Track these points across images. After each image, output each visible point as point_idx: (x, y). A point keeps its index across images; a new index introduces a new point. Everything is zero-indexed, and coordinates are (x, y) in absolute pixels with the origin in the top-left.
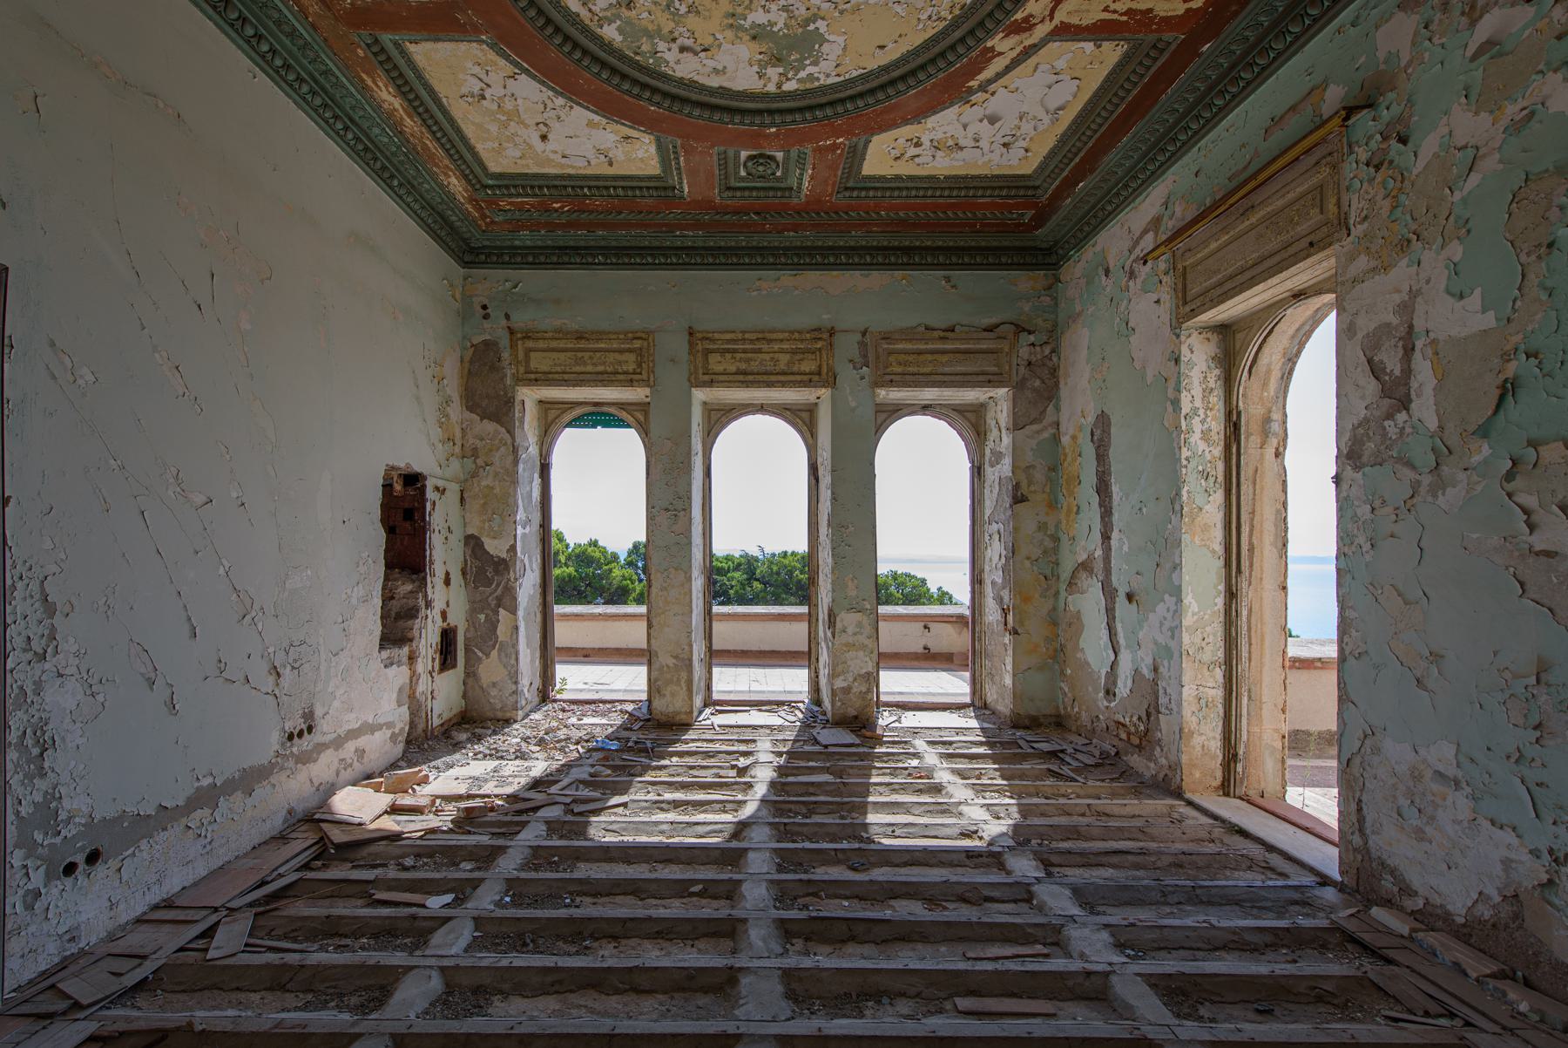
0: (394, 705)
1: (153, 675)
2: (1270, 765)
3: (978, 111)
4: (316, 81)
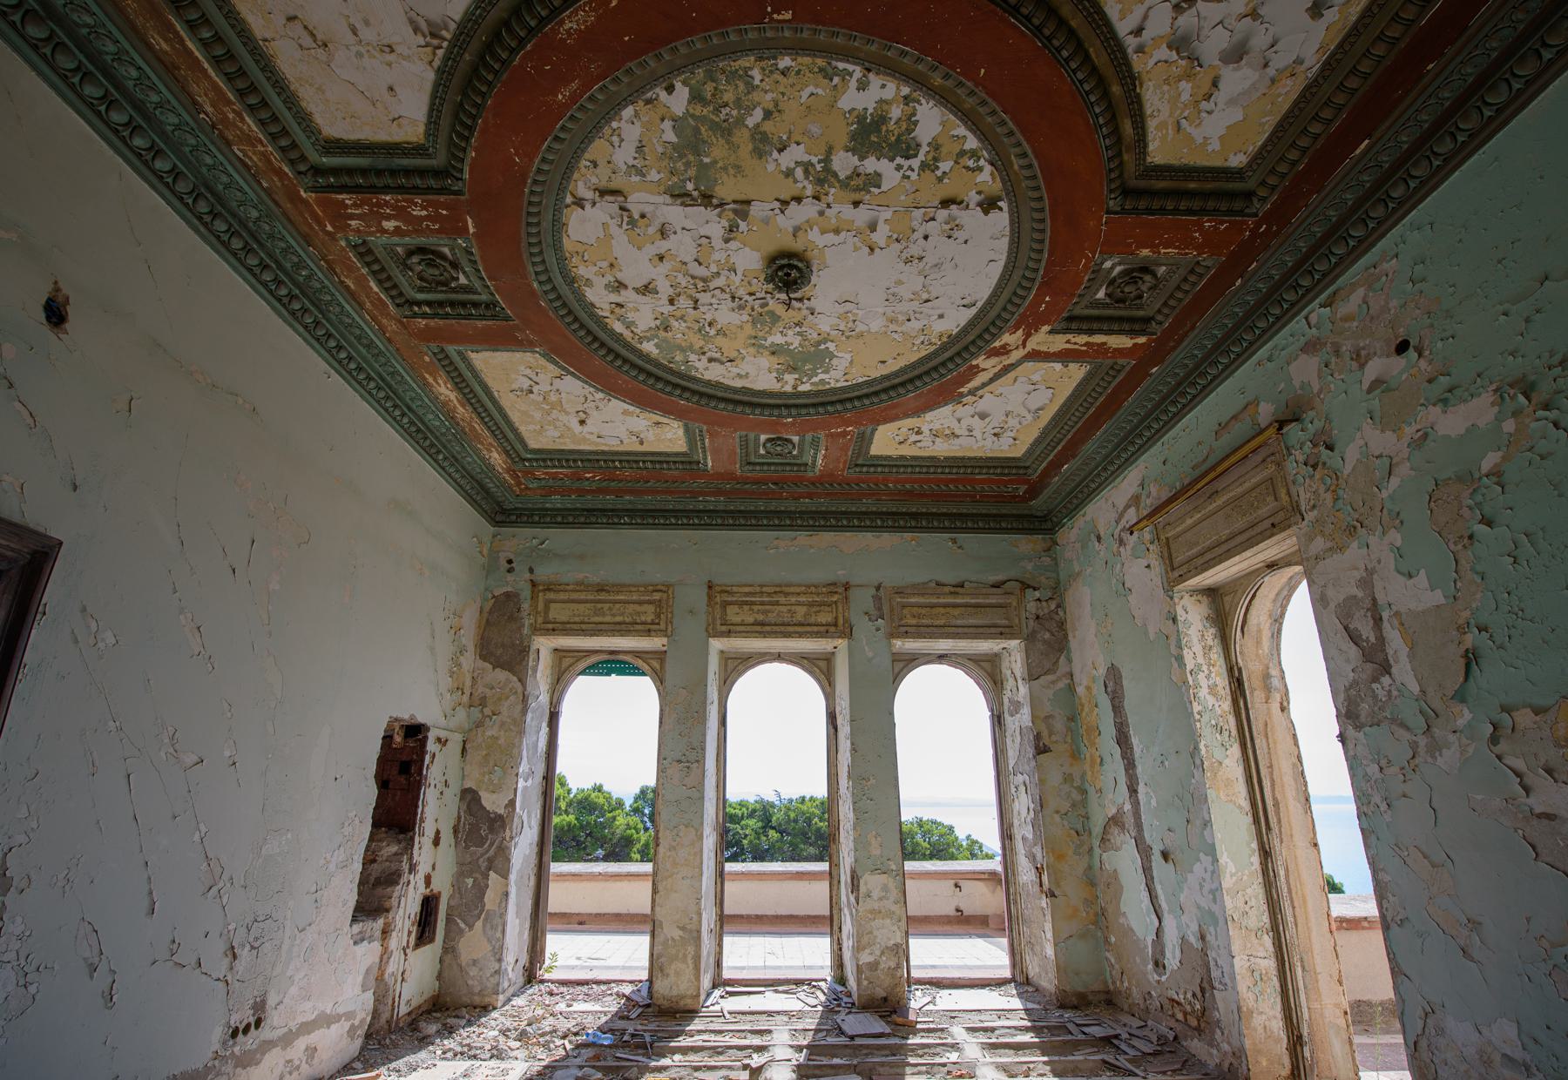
0: (358, 990)
1: (96, 960)
2: (1337, 1048)
3: (969, 410)
4: (383, 380)
